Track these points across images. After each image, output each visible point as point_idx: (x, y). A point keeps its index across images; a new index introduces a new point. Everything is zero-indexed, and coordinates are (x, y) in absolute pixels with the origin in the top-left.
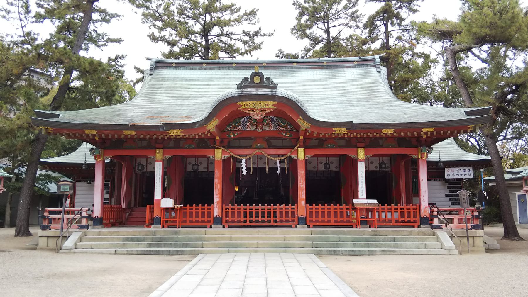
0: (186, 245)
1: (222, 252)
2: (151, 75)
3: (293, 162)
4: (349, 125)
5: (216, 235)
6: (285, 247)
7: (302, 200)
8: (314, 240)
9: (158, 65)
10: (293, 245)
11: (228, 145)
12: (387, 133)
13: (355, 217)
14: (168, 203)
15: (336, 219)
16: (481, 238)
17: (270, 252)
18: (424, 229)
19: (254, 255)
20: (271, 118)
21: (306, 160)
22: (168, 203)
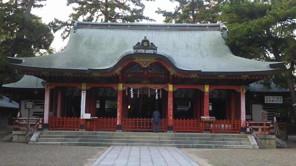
0: (103, 141)
1: (123, 145)
2: (75, 32)
3: (165, 93)
4: (199, 72)
5: (53, 145)
6: (160, 143)
7: (170, 116)
8: (178, 139)
9: (79, 25)
10: (165, 142)
11: (125, 82)
12: (221, 78)
13: (202, 127)
14: (88, 116)
15: (190, 127)
16: (274, 140)
17: (151, 146)
18: (242, 134)
19: (142, 147)
21: (173, 92)
22: (88, 116)
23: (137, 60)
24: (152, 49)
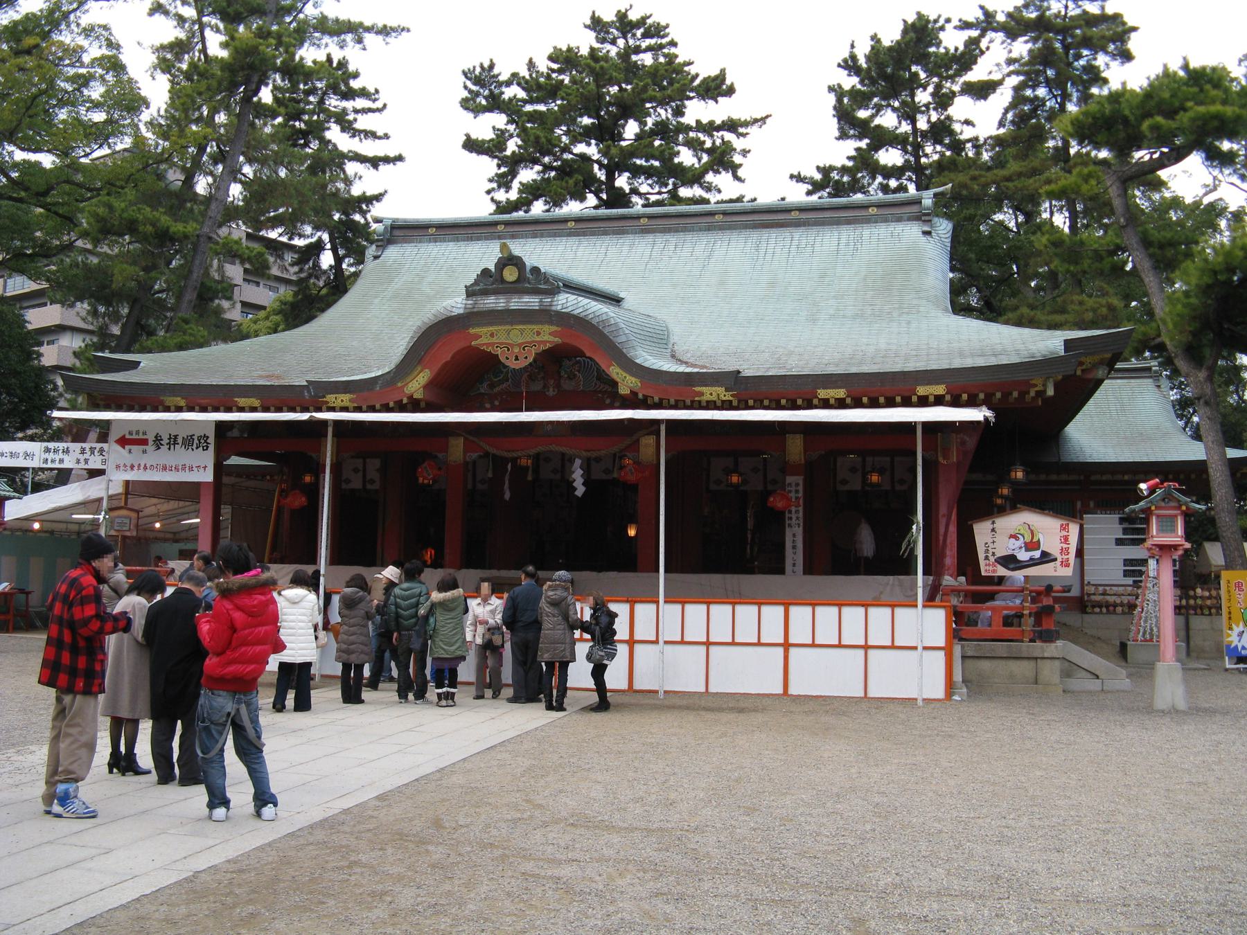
9: (396, 233)
20: (579, 362)
23: (486, 341)
24: (535, 292)
